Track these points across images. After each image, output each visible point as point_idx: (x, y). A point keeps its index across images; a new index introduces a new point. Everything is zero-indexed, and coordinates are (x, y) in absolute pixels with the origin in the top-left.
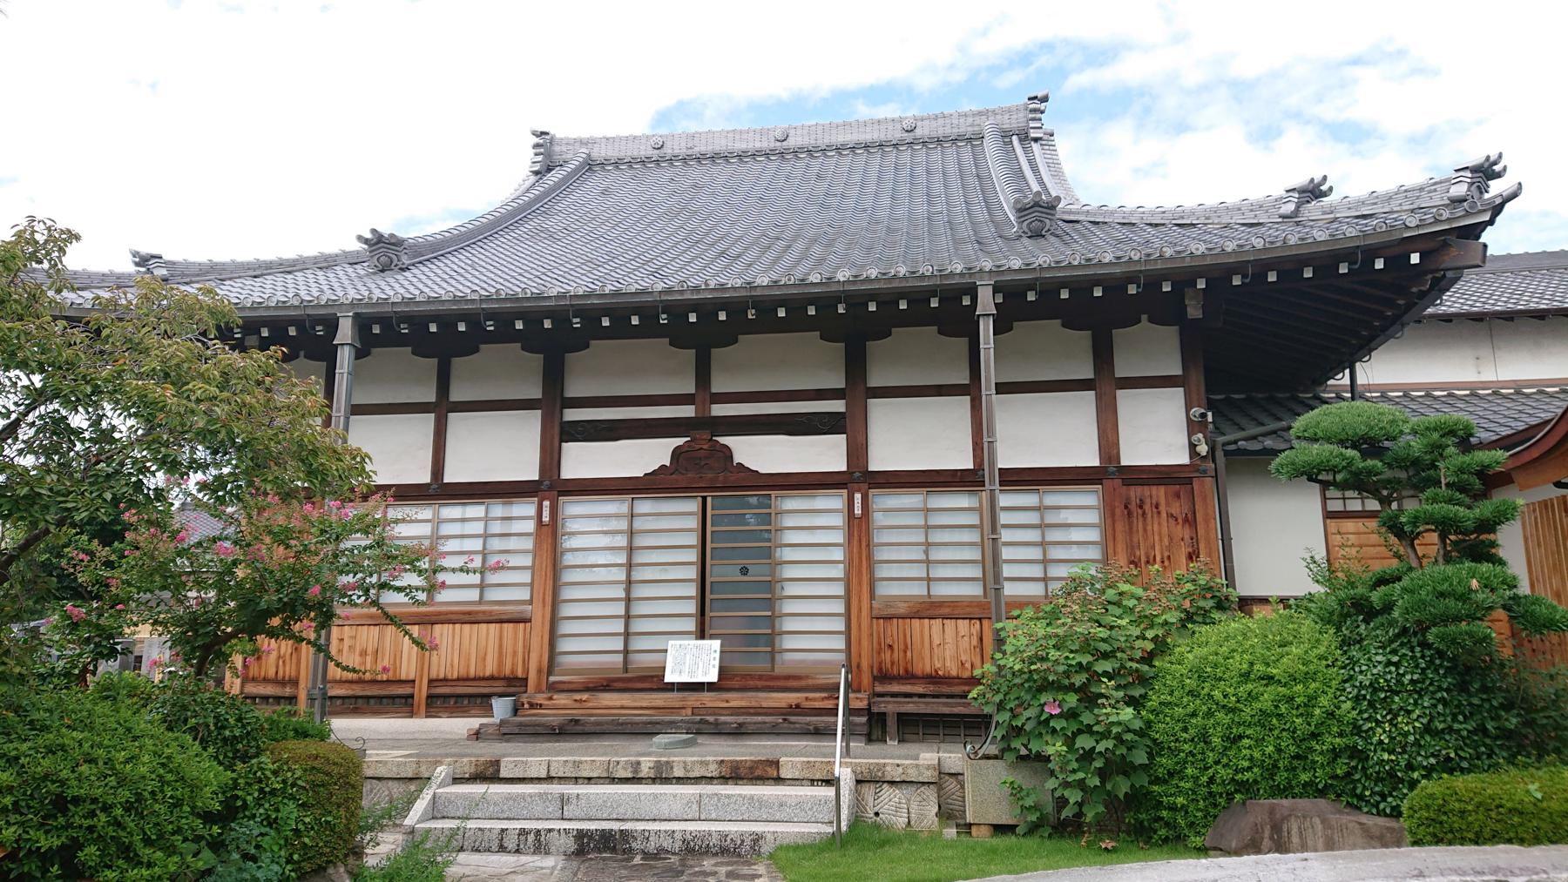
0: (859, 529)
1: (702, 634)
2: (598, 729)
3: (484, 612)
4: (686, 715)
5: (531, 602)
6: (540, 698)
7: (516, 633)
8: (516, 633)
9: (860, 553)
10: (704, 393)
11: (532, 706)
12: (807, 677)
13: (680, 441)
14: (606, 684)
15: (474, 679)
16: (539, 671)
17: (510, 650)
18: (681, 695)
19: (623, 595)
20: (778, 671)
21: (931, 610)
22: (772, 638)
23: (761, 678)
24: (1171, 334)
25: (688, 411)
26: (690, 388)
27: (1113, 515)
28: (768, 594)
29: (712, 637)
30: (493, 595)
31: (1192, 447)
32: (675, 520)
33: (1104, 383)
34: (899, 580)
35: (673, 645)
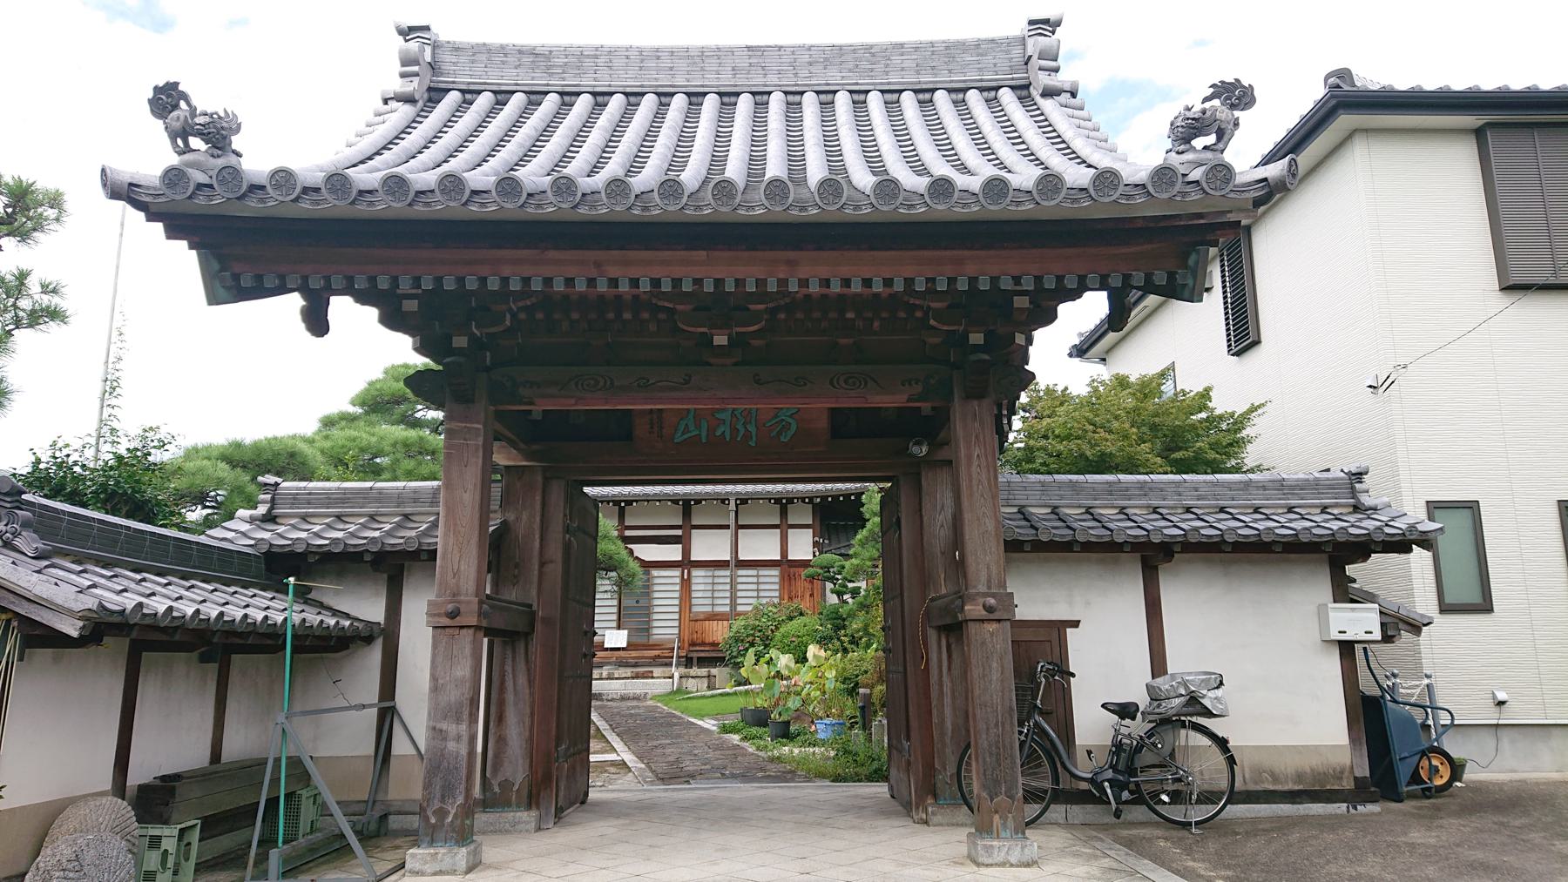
1: (619, 628)
34: (701, 605)
35: (607, 632)
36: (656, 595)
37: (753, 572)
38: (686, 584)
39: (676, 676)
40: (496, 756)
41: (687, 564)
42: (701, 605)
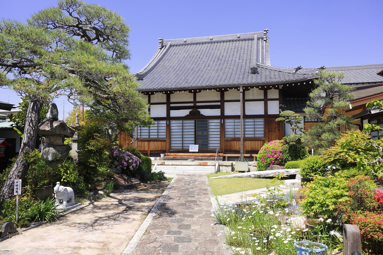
1: (195, 144)
5: (166, 138)
13: (191, 110)
15: (356, 100)
25: (192, 104)
30: (160, 137)
32: (190, 124)
34: (229, 134)
35: (190, 145)
36: (210, 130)
37: (252, 120)
38: (223, 126)
39: (217, 165)
40: (378, 96)
41: (223, 117)
42: (229, 134)
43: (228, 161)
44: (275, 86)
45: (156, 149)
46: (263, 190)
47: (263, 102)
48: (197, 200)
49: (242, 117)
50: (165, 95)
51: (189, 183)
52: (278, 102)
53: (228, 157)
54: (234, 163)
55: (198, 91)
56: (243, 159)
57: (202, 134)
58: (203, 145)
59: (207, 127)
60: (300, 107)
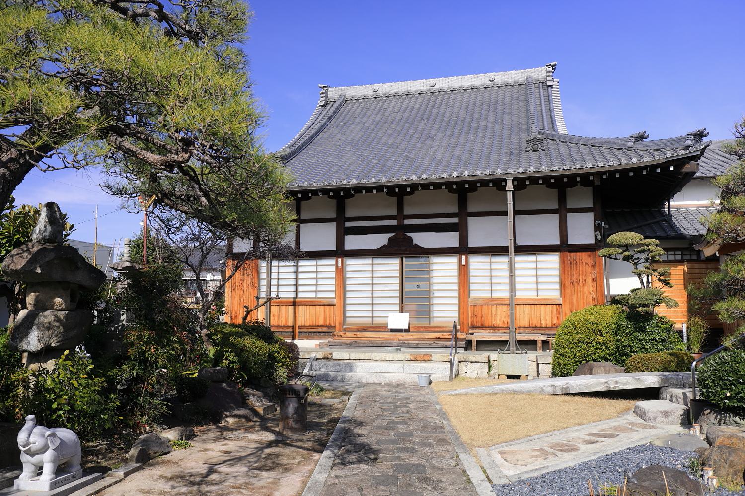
0: (464, 271)
1: (402, 312)
2: (365, 345)
3: (318, 301)
4: (396, 341)
5: (335, 298)
6: (341, 334)
7: (330, 309)
8: (330, 309)
9: (464, 280)
10: (401, 216)
11: (338, 336)
12: (443, 327)
13: (391, 235)
14: (364, 329)
15: (315, 326)
16: (340, 324)
17: (328, 316)
18: (394, 333)
19: (371, 296)
20: (432, 325)
21: (491, 302)
22: (429, 313)
23: (425, 327)
24: (589, 190)
25: (394, 222)
26: (394, 212)
27: (564, 263)
28: (427, 296)
29: (406, 312)
30: (320, 295)
31: (596, 236)
32: (390, 267)
33: (563, 211)
34: (479, 290)
35: (390, 315)
42: (479, 290)
43: (477, 349)
44: (584, 179)
45: (313, 322)
46: (595, 431)
47: (557, 216)
48: (424, 463)
49: (511, 249)
50: (334, 202)
51: (392, 406)
52: (591, 215)
53: (478, 342)
54: (494, 355)
55: (409, 190)
56: (515, 348)
57: (418, 289)
58: (419, 313)
59: (428, 272)
60: (641, 226)
